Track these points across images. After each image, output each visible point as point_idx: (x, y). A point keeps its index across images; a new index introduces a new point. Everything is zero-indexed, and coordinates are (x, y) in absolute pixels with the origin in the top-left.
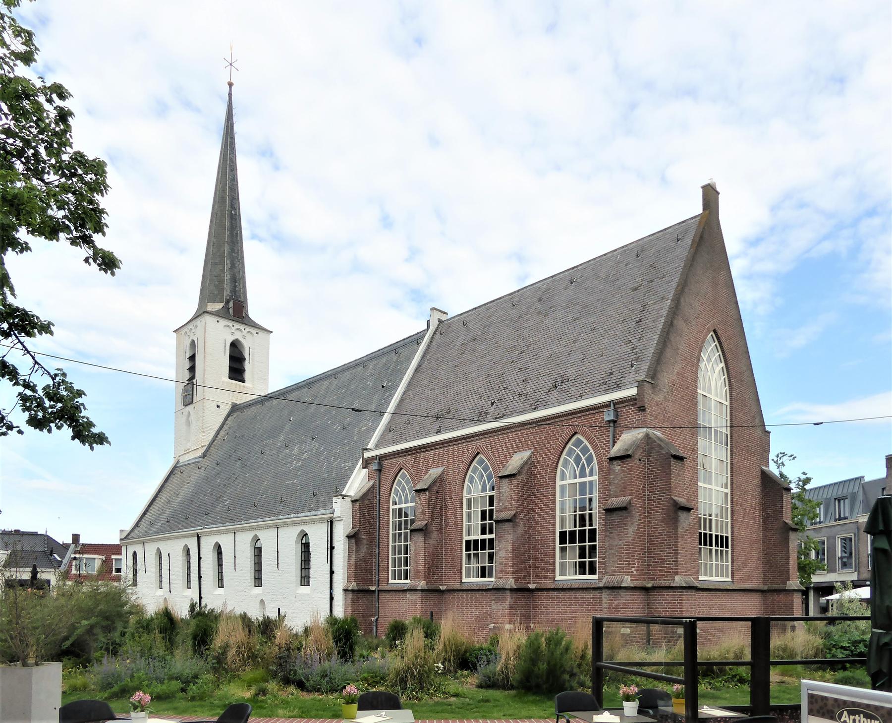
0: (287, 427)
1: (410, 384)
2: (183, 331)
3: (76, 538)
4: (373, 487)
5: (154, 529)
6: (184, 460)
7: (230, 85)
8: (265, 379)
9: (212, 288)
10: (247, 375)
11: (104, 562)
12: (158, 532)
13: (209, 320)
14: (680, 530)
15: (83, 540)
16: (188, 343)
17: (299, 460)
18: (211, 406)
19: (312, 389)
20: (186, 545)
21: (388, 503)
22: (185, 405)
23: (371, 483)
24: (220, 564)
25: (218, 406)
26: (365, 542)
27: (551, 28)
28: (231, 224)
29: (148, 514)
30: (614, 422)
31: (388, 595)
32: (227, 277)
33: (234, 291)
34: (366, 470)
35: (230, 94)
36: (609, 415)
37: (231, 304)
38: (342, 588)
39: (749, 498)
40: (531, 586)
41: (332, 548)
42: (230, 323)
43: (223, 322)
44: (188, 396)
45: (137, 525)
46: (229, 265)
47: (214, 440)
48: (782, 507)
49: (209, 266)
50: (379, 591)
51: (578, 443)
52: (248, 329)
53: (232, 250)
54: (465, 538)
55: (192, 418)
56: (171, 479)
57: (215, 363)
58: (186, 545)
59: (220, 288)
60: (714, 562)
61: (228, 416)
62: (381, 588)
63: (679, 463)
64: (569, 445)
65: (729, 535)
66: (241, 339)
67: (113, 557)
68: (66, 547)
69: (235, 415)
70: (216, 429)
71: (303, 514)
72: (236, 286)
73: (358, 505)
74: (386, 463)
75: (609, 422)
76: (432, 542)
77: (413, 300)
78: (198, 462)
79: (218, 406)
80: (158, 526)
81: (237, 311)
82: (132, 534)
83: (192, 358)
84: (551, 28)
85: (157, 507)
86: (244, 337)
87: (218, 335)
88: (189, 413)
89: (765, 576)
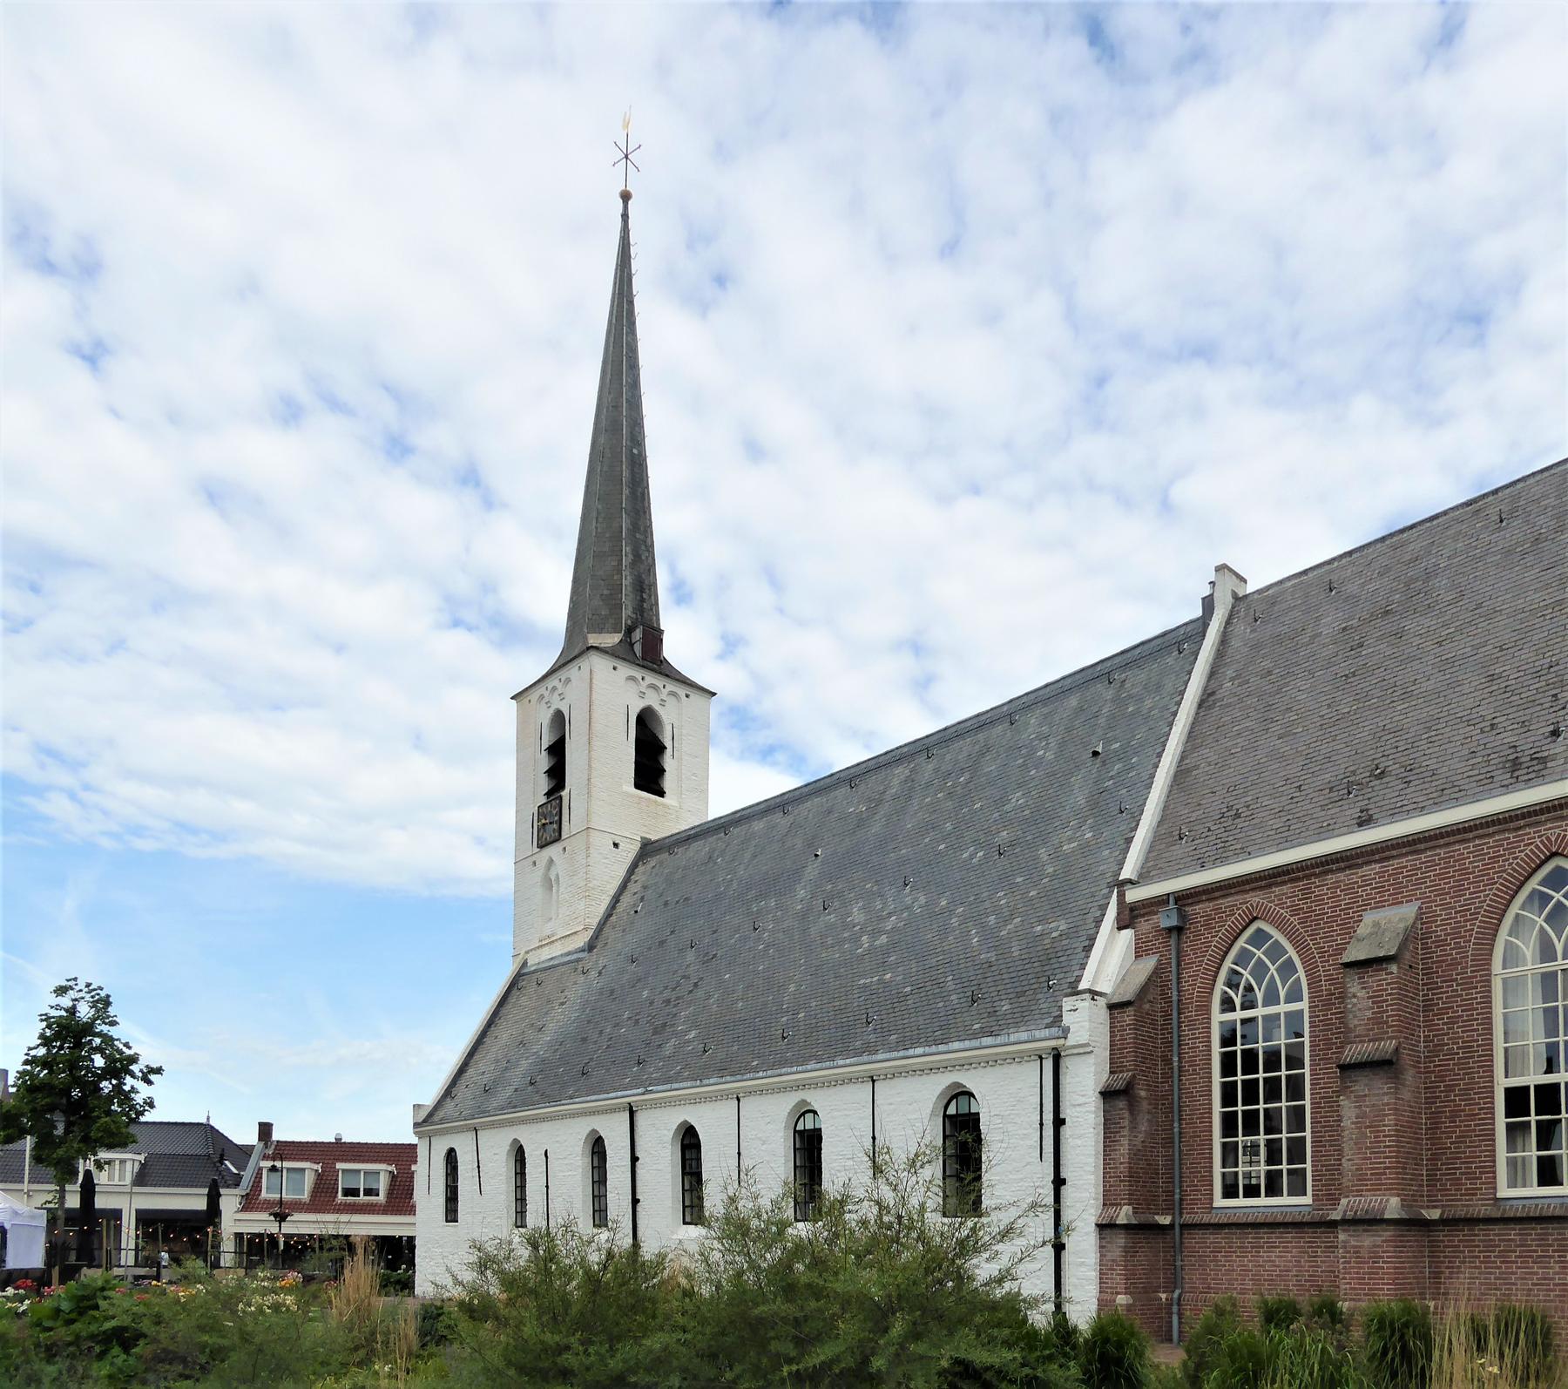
0: (812, 870)
1: (1191, 735)
2: (534, 696)
3: (265, 1130)
4: (1156, 972)
5: (494, 1103)
6: (534, 960)
7: (626, 197)
8: (702, 791)
9: (597, 602)
10: (668, 783)
11: (320, 1177)
12: (502, 1109)
13: (599, 666)
15: (277, 1135)
16: (545, 717)
17: (875, 933)
18: (602, 843)
19: (862, 787)
20: (515, 1140)
21: (1206, 1008)
22: (542, 846)
23: (1150, 963)
24: (521, 1187)
25: (616, 845)
26: (1145, 1105)
27: (950, 249)
28: (633, 473)
29: (471, 1072)
30: (1179, 930)
31: (1211, 1238)
32: (627, 581)
34: (1128, 934)
35: (625, 217)
36: (1167, 919)
37: (638, 635)
38: (1093, 1220)
41: (1059, 1122)
42: (638, 673)
43: (625, 670)
44: (549, 824)
45: (448, 1093)
47: (608, 915)
49: (589, 562)
50: (1183, 1226)
51: (1260, 938)
54: (1502, 1083)
55: (560, 867)
56: (512, 1000)
57: (604, 760)
58: (515, 1140)
61: (634, 866)
62: (1188, 1218)
64: (1241, 943)
66: (657, 707)
67: (339, 1166)
68: (246, 1151)
69: (653, 862)
70: (612, 892)
71: (956, 1045)
72: (642, 600)
73: (1128, 1017)
74: (1199, 909)
75: (1170, 930)
76: (1406, 1095)
77: (733, 726)
78: (578, 960)
79: (616, 845)
80: (506, 1093)
81: (645, 650)
82: (440, 1114)
83: (557, 750)
84: (950, 249)
85: (491, 1056)
86: (663, 703)
87: (610, 696)
88: (551, 861)
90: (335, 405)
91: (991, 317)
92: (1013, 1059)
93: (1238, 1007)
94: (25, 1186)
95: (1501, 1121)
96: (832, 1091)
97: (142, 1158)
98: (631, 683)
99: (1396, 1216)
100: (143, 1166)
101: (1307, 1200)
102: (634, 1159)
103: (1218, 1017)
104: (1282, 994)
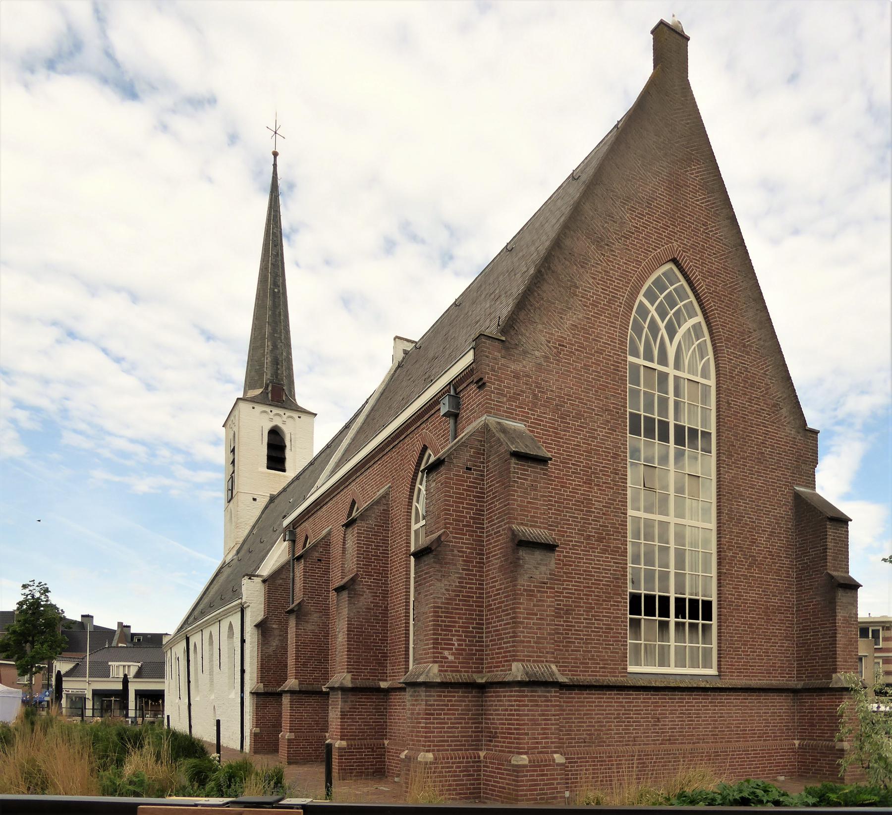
7: (275, 154)
14: (521, 581)
26: (276, 632)
28: (274, 302)
32: (268, 360)
33: (276, 374)
35: (275, 165)
37: (270, 388)
39: (762, 540)
40: (383, 685)
42: (268, 409)
43: (259, 408)
46: (271, 347)
48: (825, 550)
52: (289, 413)
53: (274, 331)
59: (261, 374)
60: (672, 643)
61: (266, 508)
63: (532, 471)
65: (714, 599)
66: (280, 425)
70: (252, 524)
72: (278, 369)
76: (309, 627)
79: (255, 499)
86: (284, 422)
87: (259, 421)
89: (800, 666)
90: (414, 238)
91: (817, 118)
94: (87, 679)
97: (139, 664)
98: (264, 414)
99: (350, 685)
100: (140, 669)
101: (713, 671)
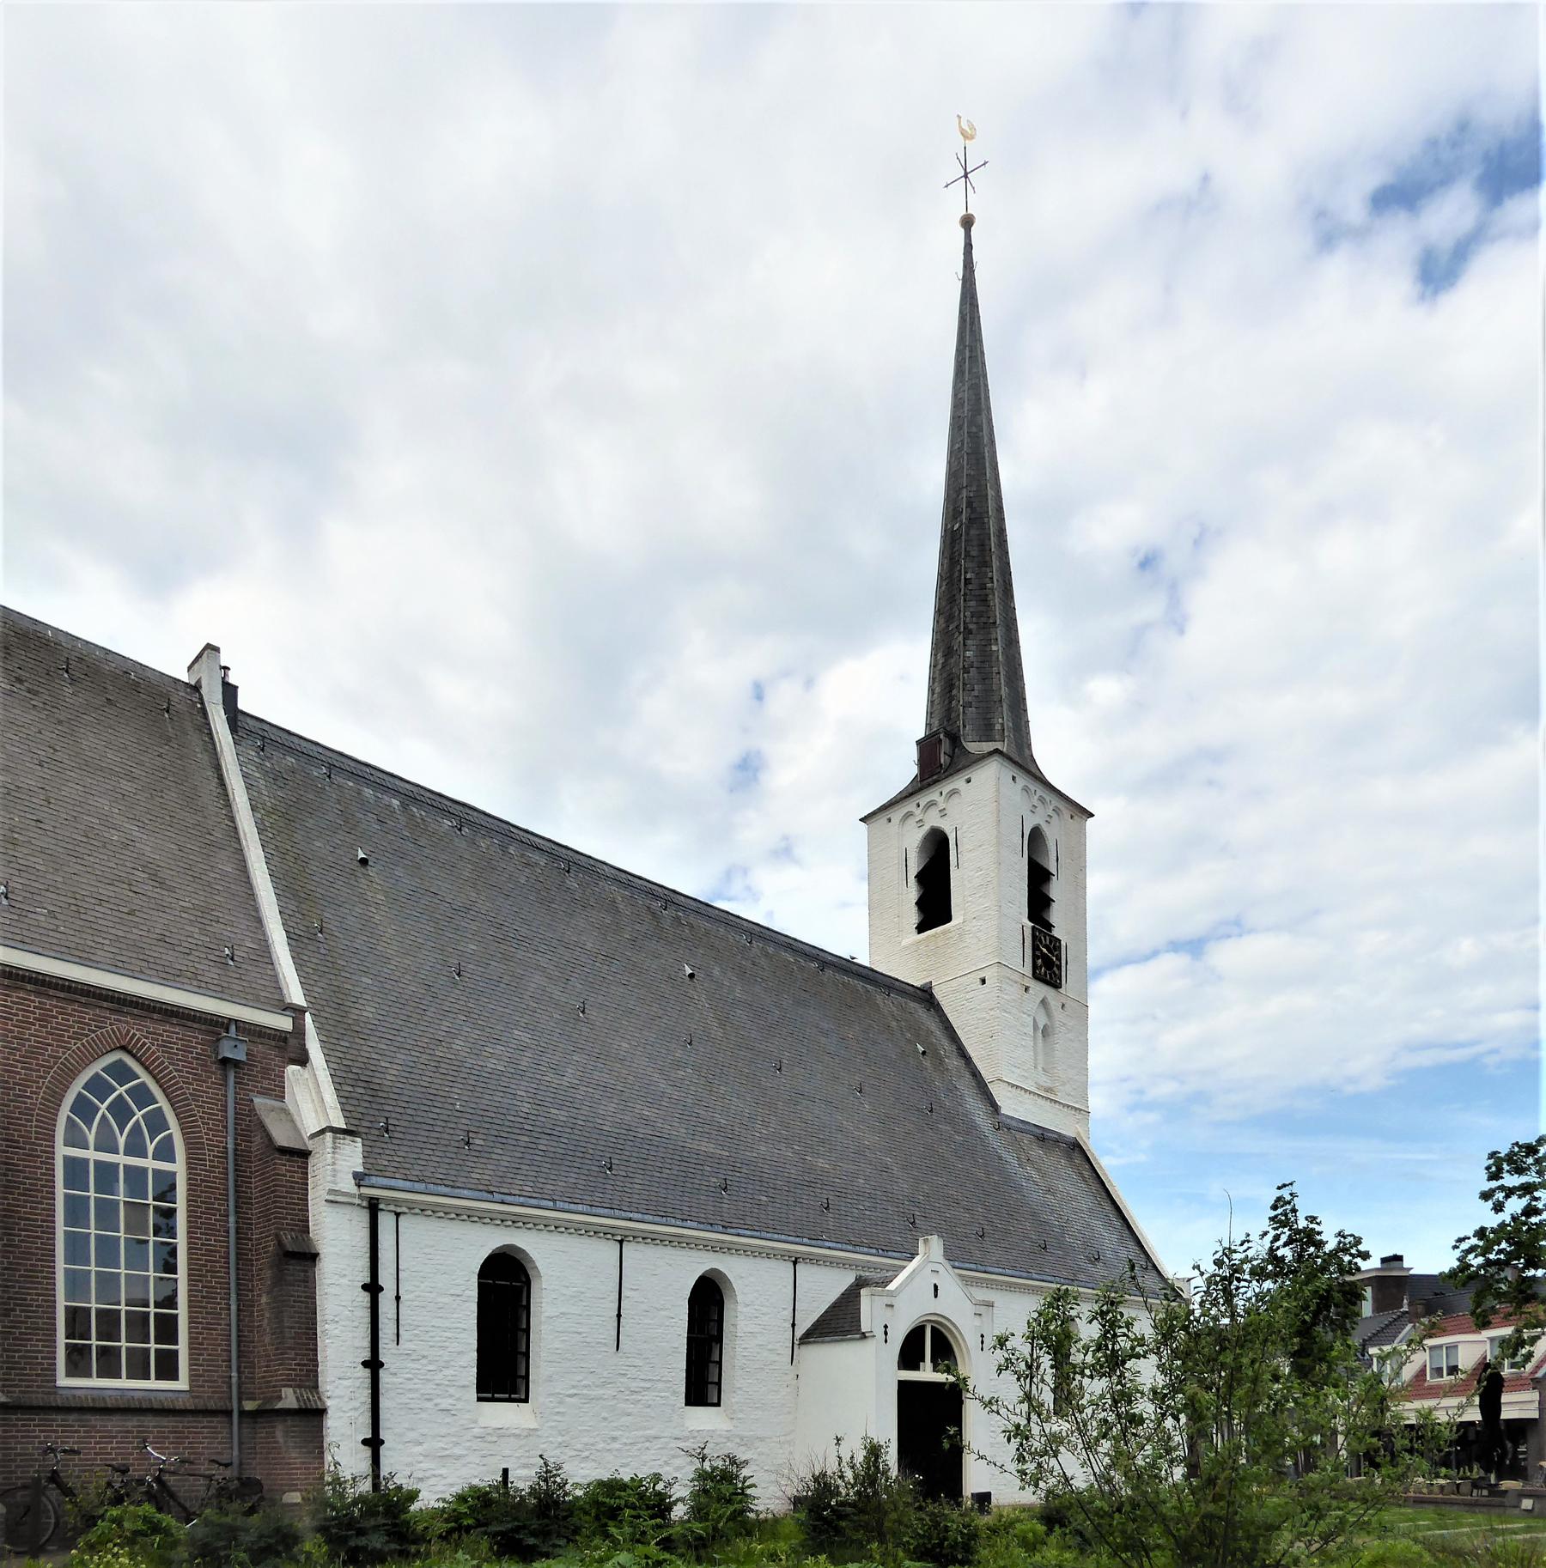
7: (967, 222)
35: (968, 246)
92: (770, 1255)
93: (150, 1154)
95: (182, 1311)
96: (585, 1240)
102: (619, 1316)
103: (62, 1151)
104: (151, 1148)
